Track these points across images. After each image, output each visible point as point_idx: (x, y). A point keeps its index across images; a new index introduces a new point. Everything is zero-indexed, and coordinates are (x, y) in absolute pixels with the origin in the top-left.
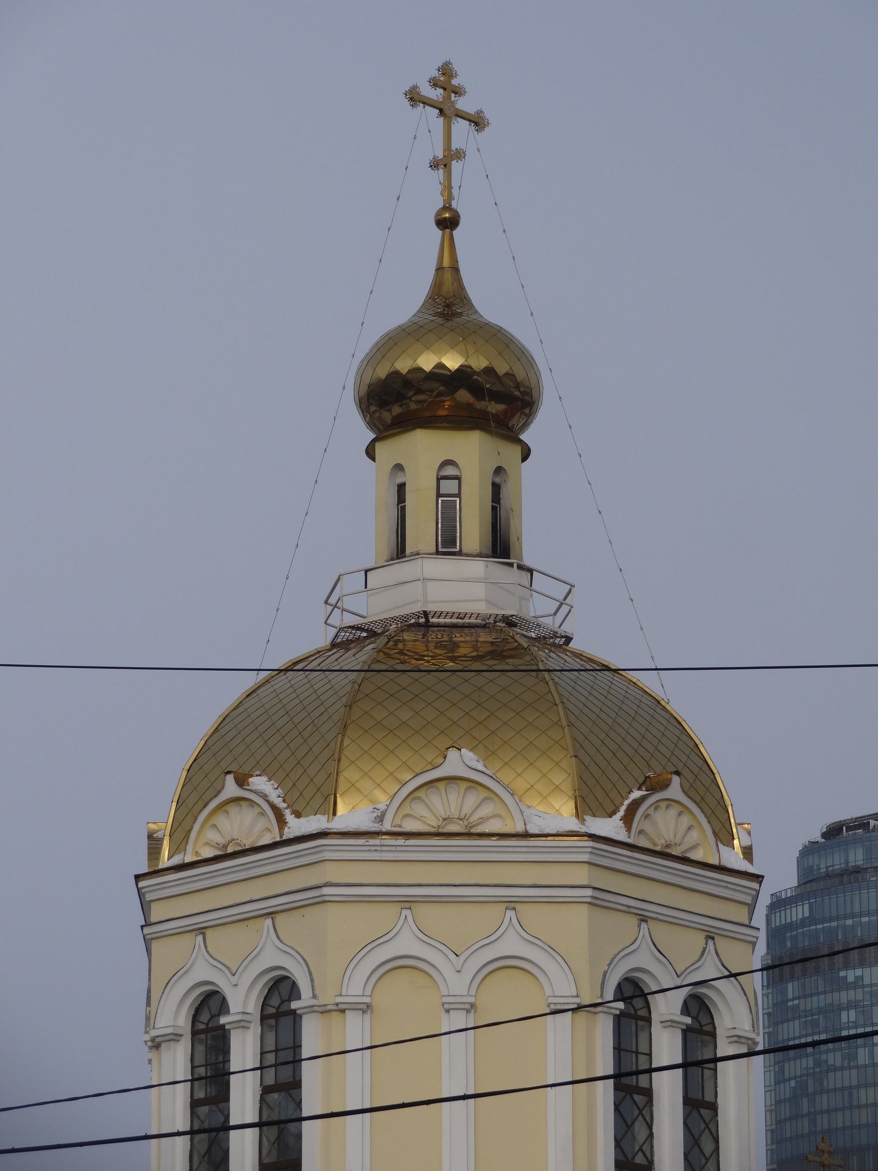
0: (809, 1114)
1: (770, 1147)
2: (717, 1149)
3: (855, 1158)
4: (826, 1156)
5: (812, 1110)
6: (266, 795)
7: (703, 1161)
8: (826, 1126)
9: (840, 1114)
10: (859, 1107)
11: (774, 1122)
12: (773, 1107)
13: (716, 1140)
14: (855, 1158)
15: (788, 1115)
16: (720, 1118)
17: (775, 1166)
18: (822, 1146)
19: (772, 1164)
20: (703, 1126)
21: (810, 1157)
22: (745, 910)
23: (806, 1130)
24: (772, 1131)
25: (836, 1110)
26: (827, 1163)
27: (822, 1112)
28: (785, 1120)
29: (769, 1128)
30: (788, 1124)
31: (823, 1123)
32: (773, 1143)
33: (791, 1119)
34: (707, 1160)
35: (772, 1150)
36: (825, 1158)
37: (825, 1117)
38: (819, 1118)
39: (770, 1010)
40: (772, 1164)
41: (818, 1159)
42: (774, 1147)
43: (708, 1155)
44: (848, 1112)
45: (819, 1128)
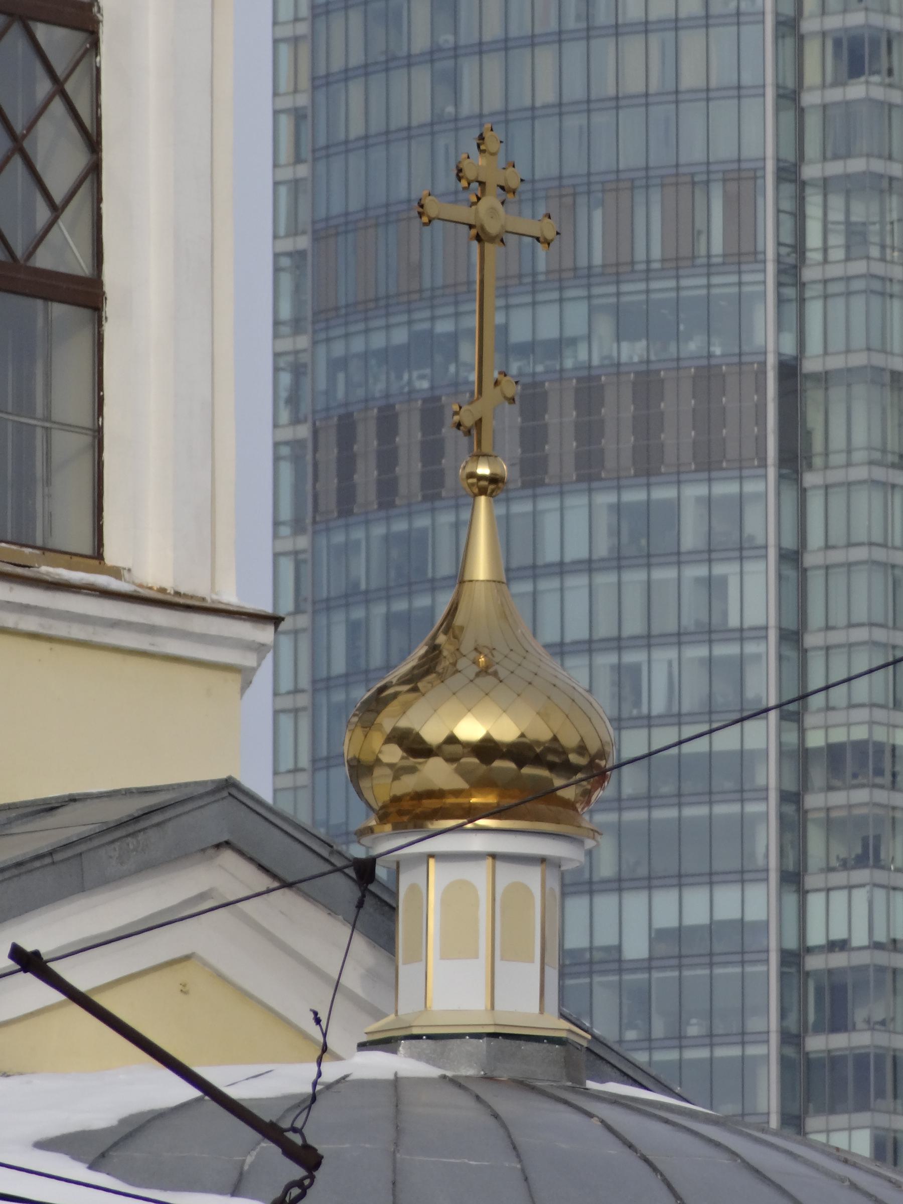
0: (433, 54)
1: (287, 174)
2: (94, 170)
3: (598, 215)
4: (490, 201)
5: (446, 39)
6: (90, 839)
7: (43, 214)
8: (494, 102)
9: (546, 58)
10: (617, 30)
11: (305, 82)
12: (303, 28)
13: (93, 142)
14: (598, 215)
15: (357, 58)
16: (106, 59)
17: (303, 242)
18: (478, 165)
19: (294, 231)
20: (44, 87)
21: (433, 207)
22: (291, 766)
23: (422, 114)
24: (298, 115)
25: (532, 42)
26: (493, 228)
27: (480, 49)
28: (347, 75)
29: (286, 102)
30: (356, 89)
31: (483, 87)
32: (298, 160)
33: (366, 70)
34: (56, 210)
35: (296, 184)
36: (490, 212)
37: (493, 64)
38: (469, 69)
39: (303, 100)
40: (294, 231)
41: (463, 213)
42: (303, 171)
43: (58, 196)
44: (574, 51)
45: (468, 106)
